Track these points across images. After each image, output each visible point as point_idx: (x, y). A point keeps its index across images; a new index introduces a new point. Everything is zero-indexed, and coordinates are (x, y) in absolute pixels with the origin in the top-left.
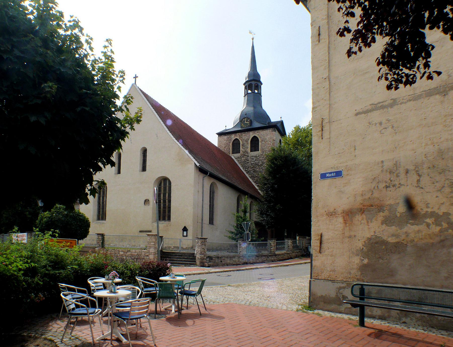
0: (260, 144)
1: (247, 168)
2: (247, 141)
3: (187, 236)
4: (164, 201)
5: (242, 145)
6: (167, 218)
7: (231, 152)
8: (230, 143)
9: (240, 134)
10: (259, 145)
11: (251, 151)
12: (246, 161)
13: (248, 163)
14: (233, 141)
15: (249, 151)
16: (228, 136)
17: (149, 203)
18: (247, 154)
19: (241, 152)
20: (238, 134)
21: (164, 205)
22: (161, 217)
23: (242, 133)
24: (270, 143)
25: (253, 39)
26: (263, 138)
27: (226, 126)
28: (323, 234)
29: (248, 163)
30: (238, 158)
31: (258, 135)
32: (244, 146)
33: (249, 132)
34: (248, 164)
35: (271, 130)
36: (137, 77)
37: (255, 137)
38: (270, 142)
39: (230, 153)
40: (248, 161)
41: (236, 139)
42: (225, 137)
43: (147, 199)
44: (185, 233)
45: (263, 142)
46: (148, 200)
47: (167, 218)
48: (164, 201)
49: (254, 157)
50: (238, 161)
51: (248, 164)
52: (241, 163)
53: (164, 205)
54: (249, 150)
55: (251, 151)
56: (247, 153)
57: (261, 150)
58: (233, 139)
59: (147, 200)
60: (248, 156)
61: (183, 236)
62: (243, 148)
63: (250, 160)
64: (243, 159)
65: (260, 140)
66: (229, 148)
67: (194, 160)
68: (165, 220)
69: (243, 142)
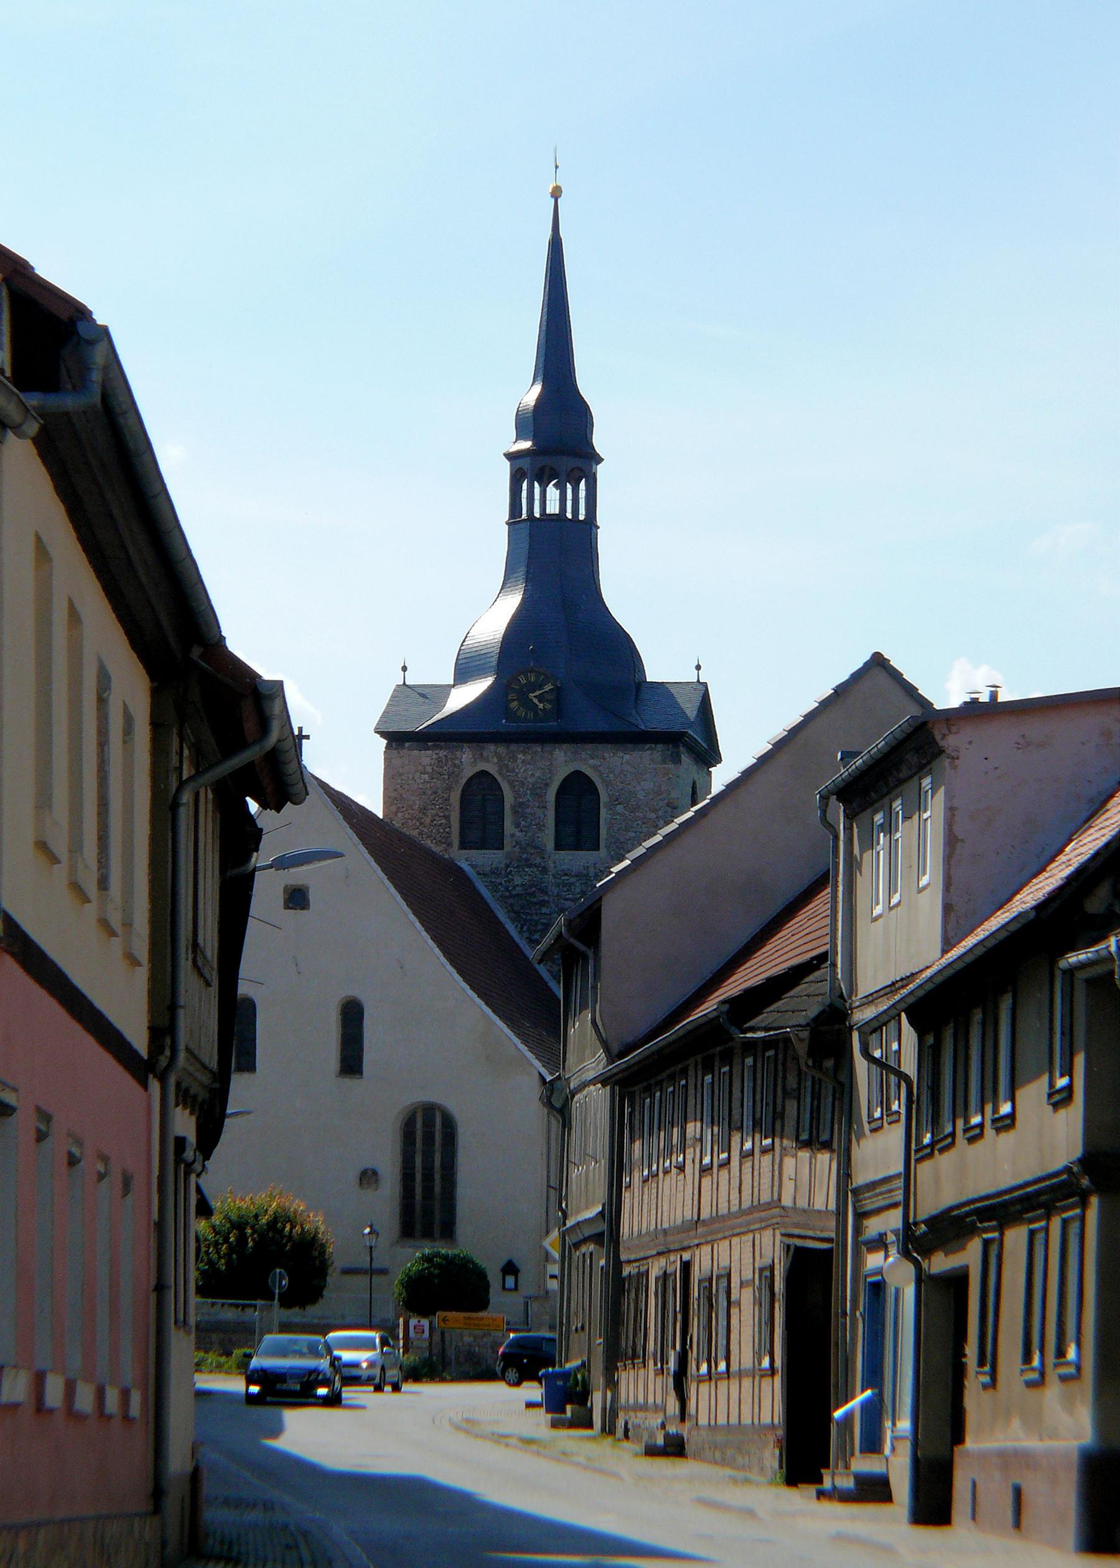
0: (604, 813)
1: (540, 927)
2: (538, 792)
3: (516, 1288)
4: (428, 1177)
5: (513, 807)
6: (437, 1230)
7: (456, 842)
8: (449, 789)
9: (502, 749)
10: (602, 821)
11: (558, 847)
12: (533, 894)
13: (543, 903)
14: (463, 781)
15: (550, 845)
16: (442, 753)
17: (377, 1181)
18: (538, 861)
19: (507, 841)
20: (492, 747)
21: (428, 1189)
22: (418, 1226)
23: (514, 747)
24: (653, 816)
25: (556, 193)
26: (621, 786)
27: (404, 669)
28: (977, 1481)
29: (543, 903)
30: (495, 872)
31: (595, 768)
32: (525, 818)
33: (548, 747)
34: (544, 910)
35: (657, 756)
36: (307, 737)
37: (577, 775)
38: (655, 811)
39: (450, 845)
40: (546, 893)
41: (484, 774)
42: (427, 757)
43: (369, 1166)
44: (510, 1281)
45: (620, 808)
46: (375, 1173)
47: (437, 1230)
48: (428, 1177)
49: (572, 880)
50: (494, 887)
51: (544, 910)
52: (511, 901)
53: (428, 1189)
54: (548, 838)
55: (558, 847)
56: (541, 851)
57: (607, 847)
58: (468, 772)
59: (370, 1173)
60: (545, 870)
61: (504, 1288)
62: (517, 825)
63: (556, 891)
64: (518, 881)
65: (604, 797)
66: (447, 818)
67: (537, 1064)
68: (414, 1237)
69: (517, 795)
